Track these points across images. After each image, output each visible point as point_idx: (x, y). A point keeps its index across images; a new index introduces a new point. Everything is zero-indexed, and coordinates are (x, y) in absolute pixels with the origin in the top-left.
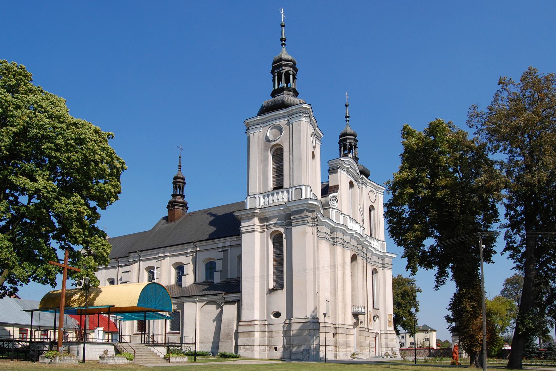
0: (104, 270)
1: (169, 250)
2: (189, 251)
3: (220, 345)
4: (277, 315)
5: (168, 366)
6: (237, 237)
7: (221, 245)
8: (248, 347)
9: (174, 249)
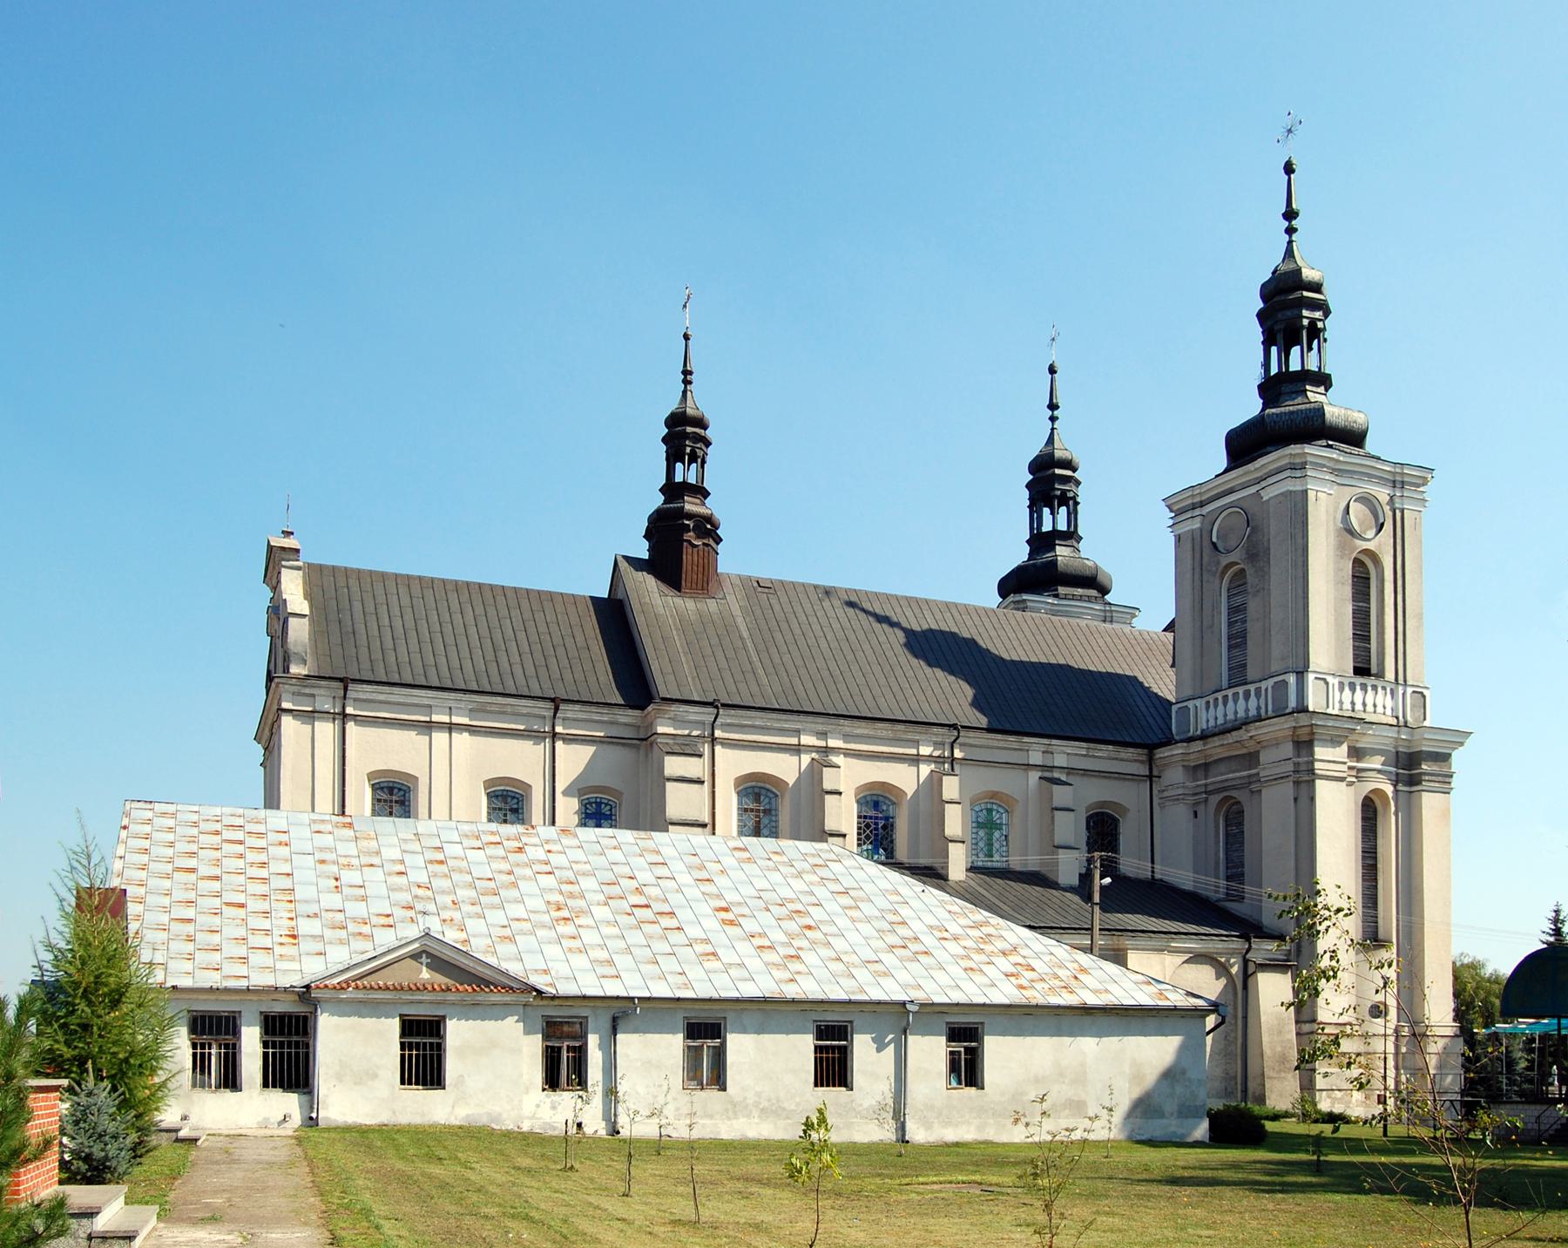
0: (466, 735)
1: (848, 729)
2: (925, 750)
3: (1267, 1086)
4: (1378, 1011)
5: (1248, 1159)
6: (1092, 745)
7: (1036, 757)
8: (1338, 1094)
9: (866, 732)
